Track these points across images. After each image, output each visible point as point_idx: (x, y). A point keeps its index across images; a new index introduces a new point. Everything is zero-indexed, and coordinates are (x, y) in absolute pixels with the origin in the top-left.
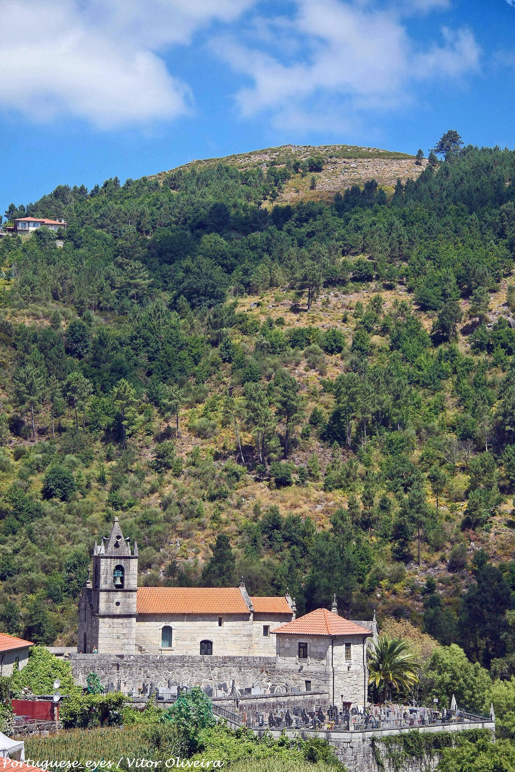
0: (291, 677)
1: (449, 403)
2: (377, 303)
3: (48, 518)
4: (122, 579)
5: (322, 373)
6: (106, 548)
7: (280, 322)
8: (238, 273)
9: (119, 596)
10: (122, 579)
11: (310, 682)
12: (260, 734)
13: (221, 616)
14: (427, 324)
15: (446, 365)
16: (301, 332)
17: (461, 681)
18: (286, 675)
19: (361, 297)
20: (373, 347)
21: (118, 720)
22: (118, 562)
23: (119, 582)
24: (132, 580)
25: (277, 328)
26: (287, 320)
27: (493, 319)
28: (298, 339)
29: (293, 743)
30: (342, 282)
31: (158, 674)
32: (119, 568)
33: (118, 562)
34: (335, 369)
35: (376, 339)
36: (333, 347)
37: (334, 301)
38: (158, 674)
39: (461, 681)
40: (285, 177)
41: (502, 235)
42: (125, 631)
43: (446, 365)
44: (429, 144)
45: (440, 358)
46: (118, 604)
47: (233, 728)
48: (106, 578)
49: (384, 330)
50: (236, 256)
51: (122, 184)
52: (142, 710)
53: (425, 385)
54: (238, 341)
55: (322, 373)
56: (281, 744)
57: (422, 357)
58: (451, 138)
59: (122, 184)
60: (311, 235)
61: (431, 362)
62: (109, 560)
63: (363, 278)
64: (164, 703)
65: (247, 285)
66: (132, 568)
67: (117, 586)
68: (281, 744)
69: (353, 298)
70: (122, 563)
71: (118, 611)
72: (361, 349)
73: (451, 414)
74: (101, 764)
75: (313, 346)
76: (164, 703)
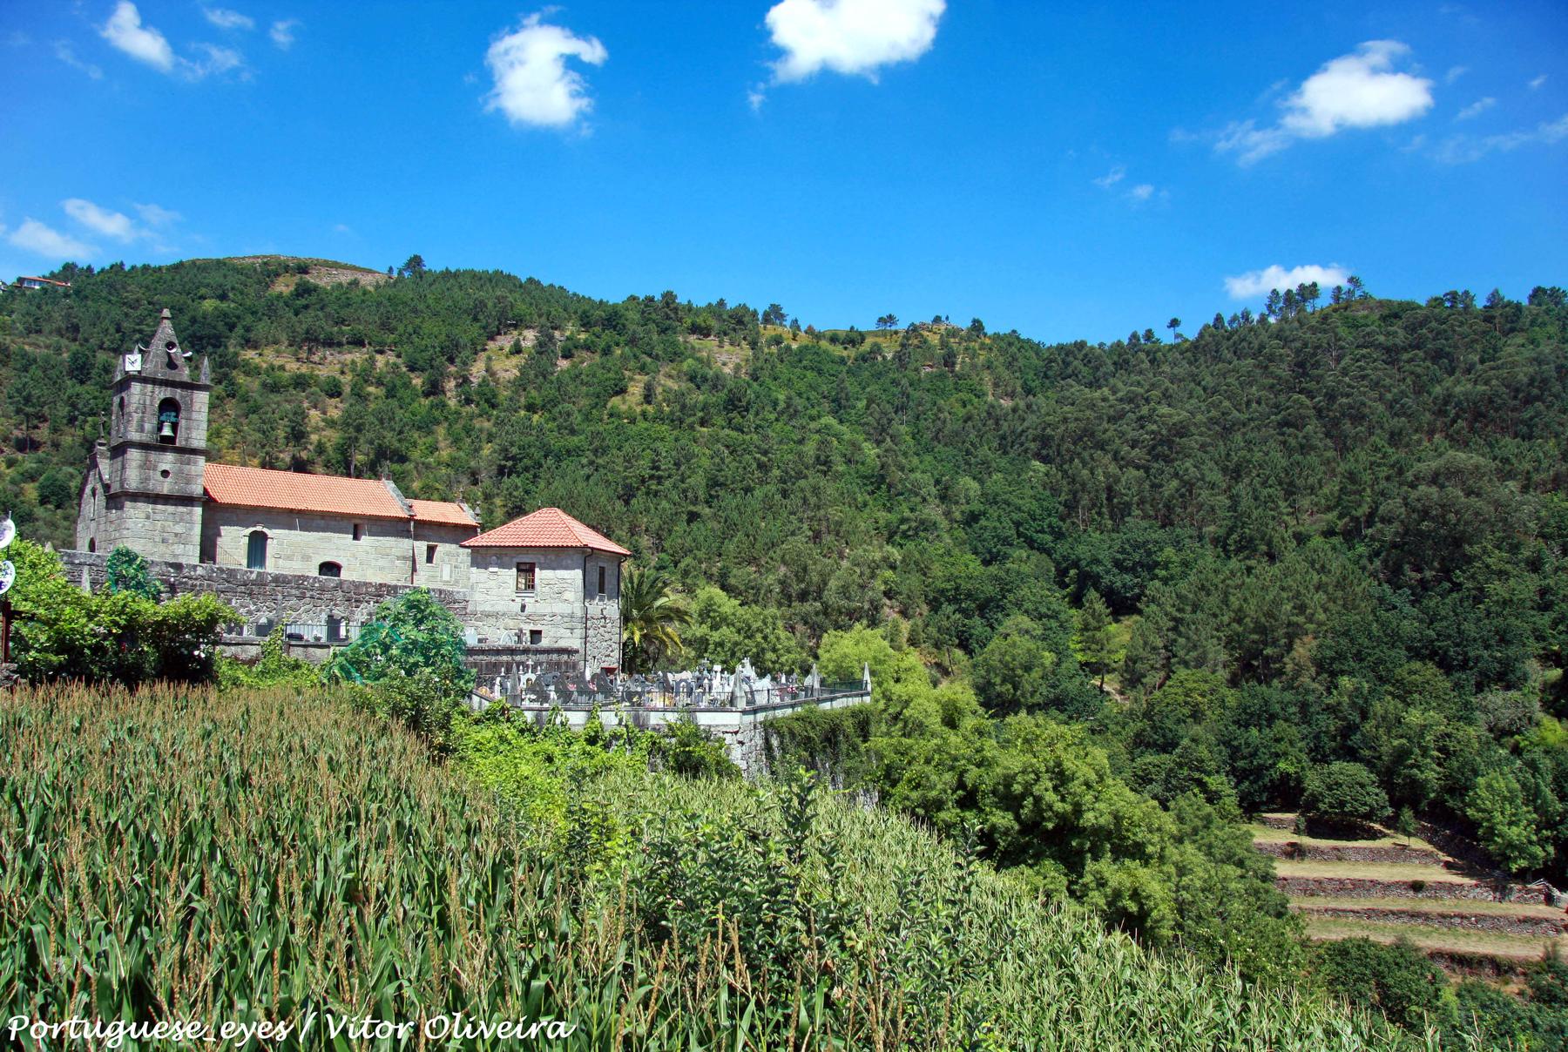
0: (501, 624)
1: (442, 445)
2: (372, 361)
3: (40, 523)
4: (175, 427)
5: (324, 413)
6: (144, 361)
7: (282, 368)
8: (239, 330)
9: (167, 460)
10: (175, 427)
11: (539, 632)
12: (538, 720)
13: (358, 521)
14: (417, 381)
15: (437, 413)
16: (302, 376)
17: (759, 637)
18: (492, 621)
19: (358, 356)
20: (369, 394)
21: (202, 673)
22: (166, 393)
23: (167, 432)
24: (197, 427)
25: (278, 373)
26: (288, 367)
27: (475, 381)
28: (300, 382)
29: (616, 737)
30: (340, 344)
31: (253, 608)
32: (169, 406)
33: (166, 393)
34: (335, 409)
35: (371, 389)
36: (334, 391)
37: (330, 358)
38: (253, 608)
39: (759, 637)
40: (278, 275)
41: (476, 319)
42: (179, 529)
43: (437, 413)
44: (399, 262)
45: (432, 406)
46: (165, 473)
47: (476, 706)
48: (142, 420)
49: (379, 383)
50: (238, 317)
51: (127, 268)
52: (252, 662)
53: (419, 428)
54: (241, 379)
55: (324, 413)
56: (592, 741)
57: (416, 405)
58: (415, 262)
59: (127, 268)
60: (306, 307)
61: (423, 411)
62: (150, 387)
63: (358, 342)
64: (305, 646)
65: (248, 341)
66: (196, 407)
67: (165, 439)
68: (592, 741)
69: (348, 357)
70: (178, 394)
71: (166, 487)
72: (360, 396)
73: (445, 454)
74: (499, 1031)
75: (314, 389)
76: (305, 646)
